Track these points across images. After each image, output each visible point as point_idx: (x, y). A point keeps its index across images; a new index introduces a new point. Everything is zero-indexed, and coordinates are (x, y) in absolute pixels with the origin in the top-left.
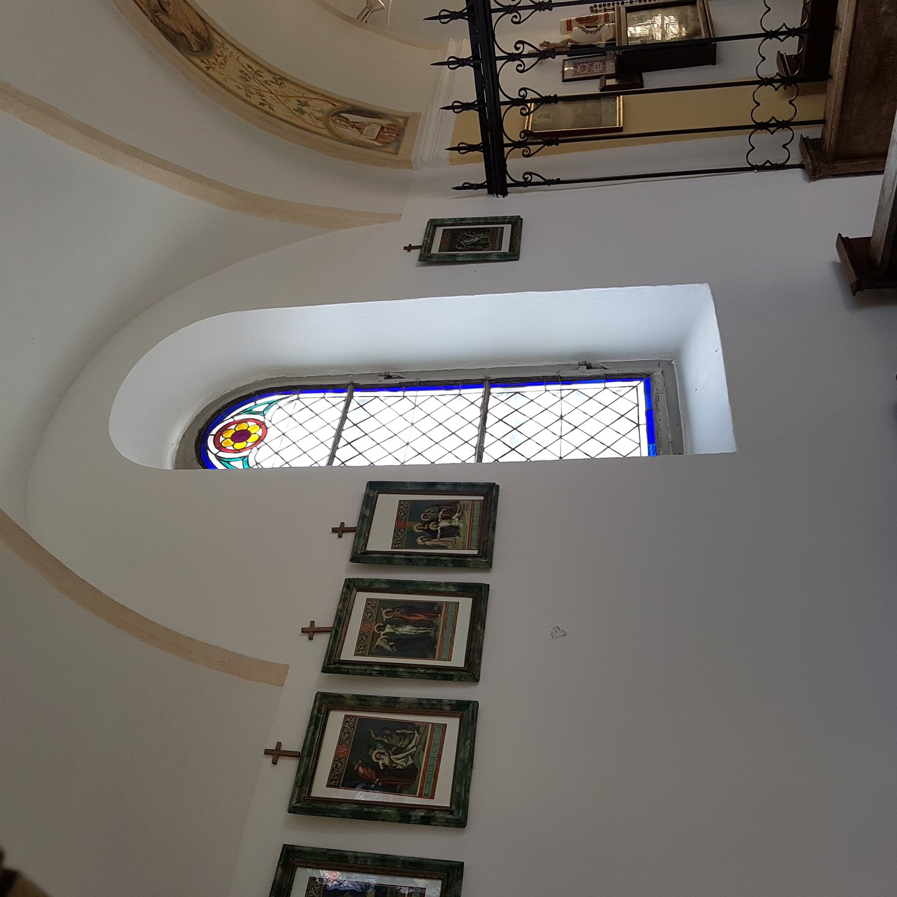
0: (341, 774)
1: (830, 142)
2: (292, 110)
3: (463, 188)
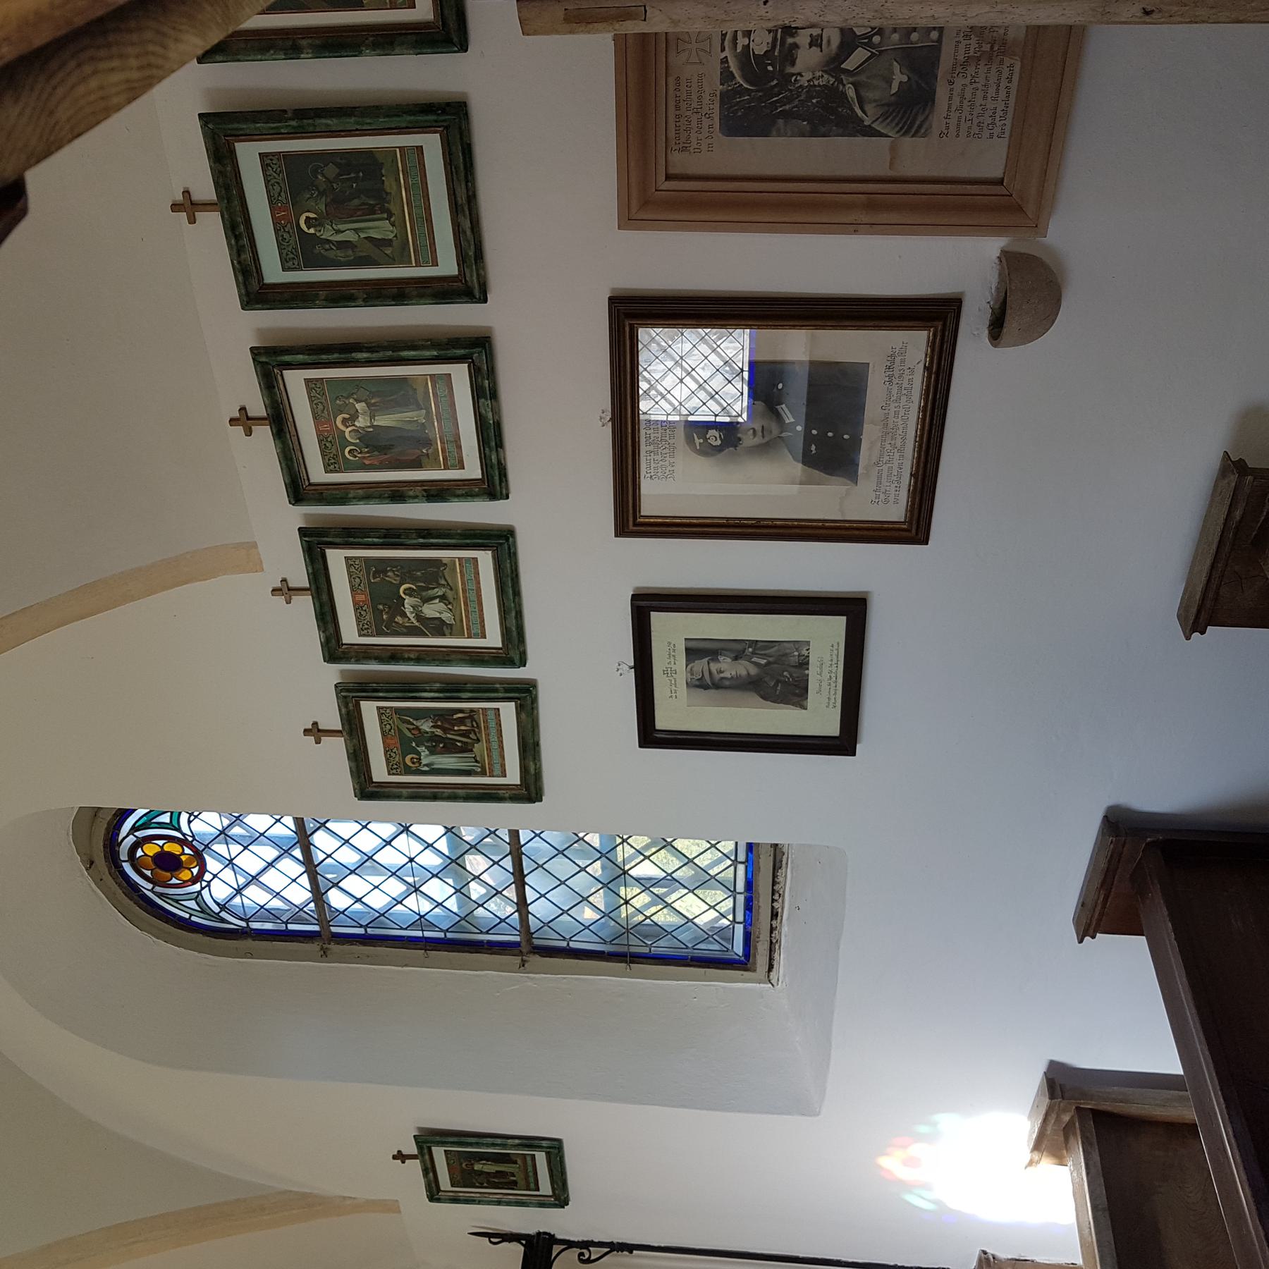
0: (296, 249)
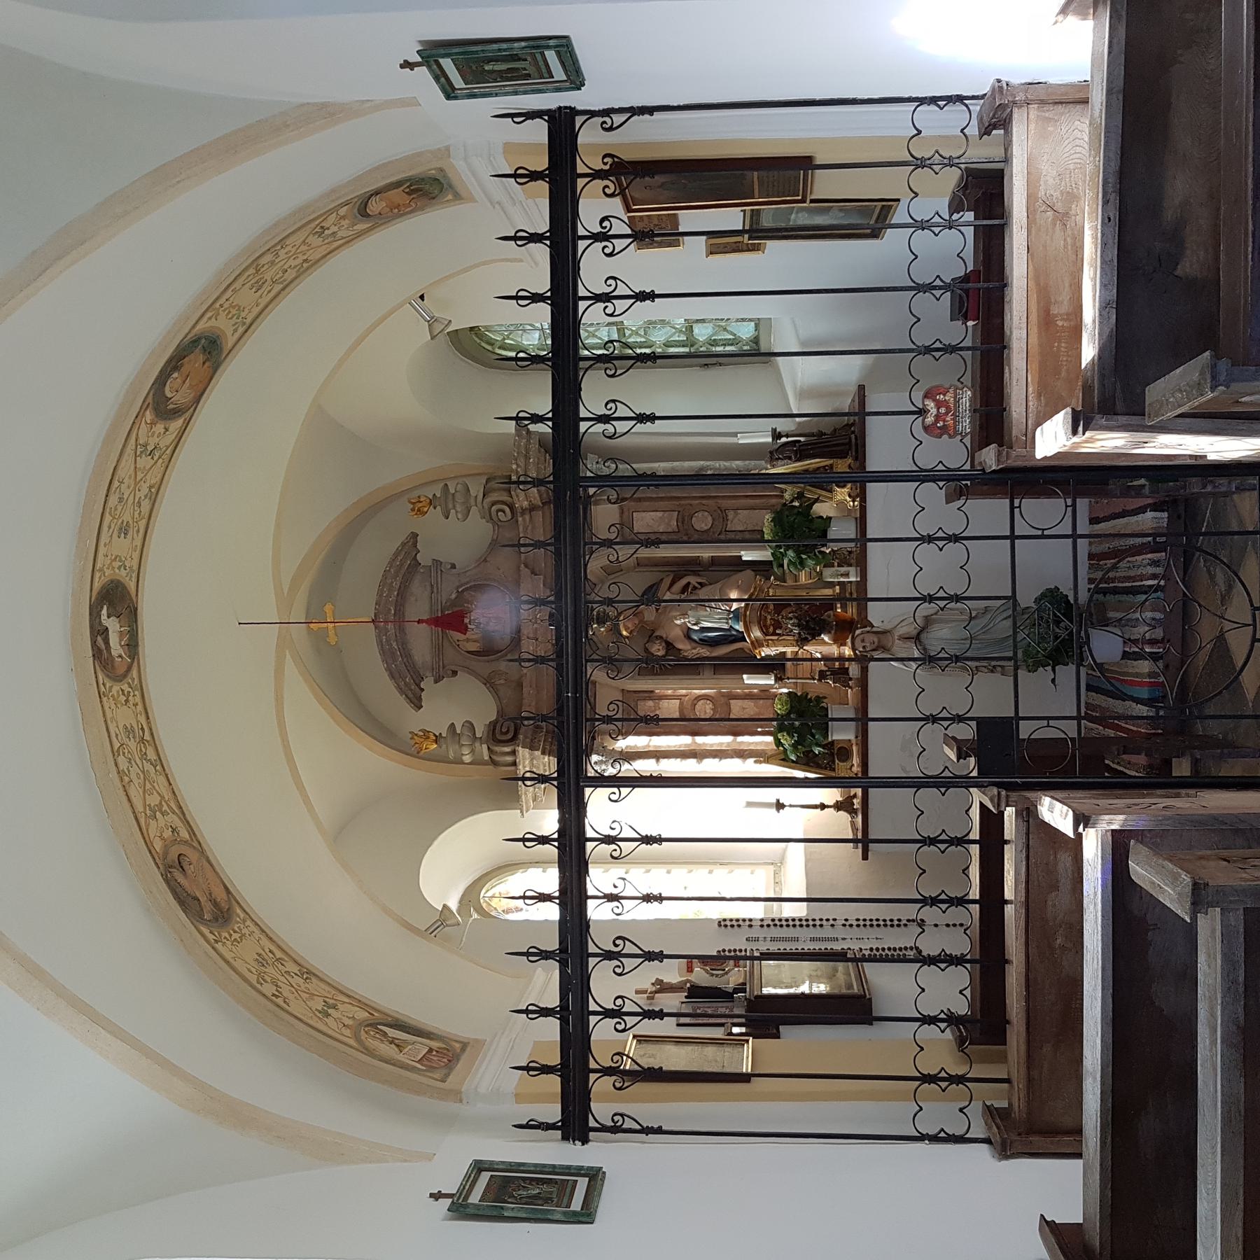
1: (1019, 1106)
2: (314, 1009)
3: (527, 1126)
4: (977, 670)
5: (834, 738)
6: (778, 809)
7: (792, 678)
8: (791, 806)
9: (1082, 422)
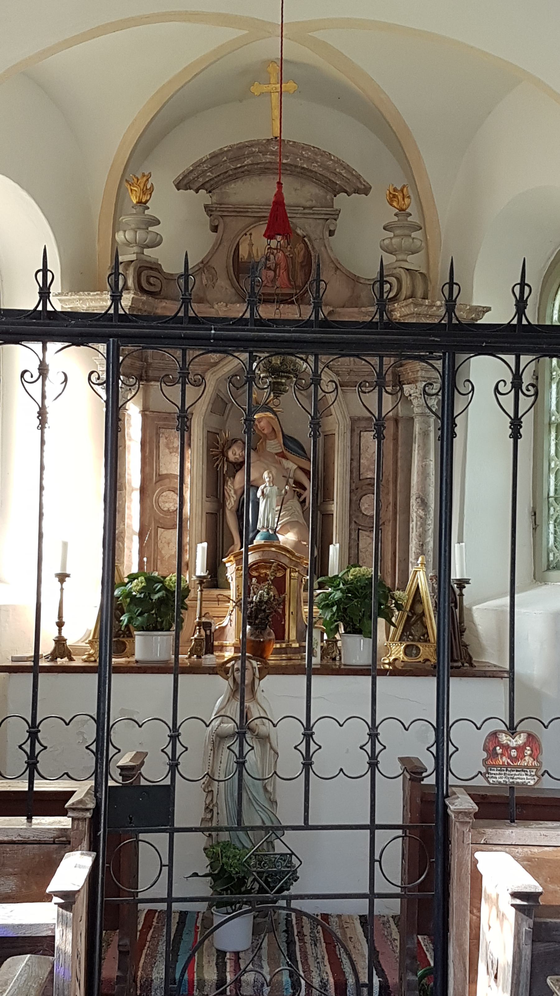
4: (209, 792)
5: (137, 639)
6: (58, 575)
7: (201, 594)
8: (62, 589)
9: (525, 903)
